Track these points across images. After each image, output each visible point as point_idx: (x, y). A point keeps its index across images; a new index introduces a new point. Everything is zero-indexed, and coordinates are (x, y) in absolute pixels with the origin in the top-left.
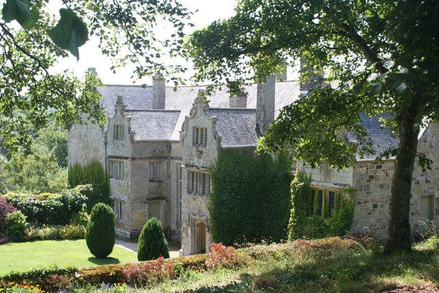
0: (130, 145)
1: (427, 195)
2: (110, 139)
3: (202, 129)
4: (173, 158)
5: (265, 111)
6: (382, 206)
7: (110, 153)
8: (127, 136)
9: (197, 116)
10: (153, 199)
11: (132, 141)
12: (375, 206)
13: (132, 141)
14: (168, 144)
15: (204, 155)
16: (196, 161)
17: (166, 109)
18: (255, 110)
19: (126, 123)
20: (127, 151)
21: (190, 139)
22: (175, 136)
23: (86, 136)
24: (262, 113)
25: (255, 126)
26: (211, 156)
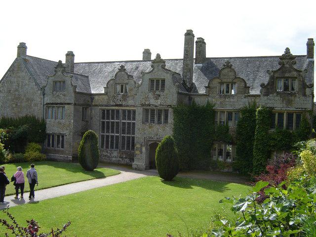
0: (73, 95)
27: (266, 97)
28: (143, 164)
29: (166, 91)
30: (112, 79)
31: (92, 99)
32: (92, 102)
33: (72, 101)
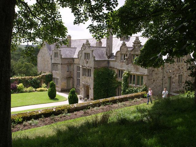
0: (60, 59)
1: (170, 76)
2: (53, 57)
3: (88, 54)
4: (75, 64)
5: (109, 48)
6: (156, 81)
7: (53, 62)
8: (60, 56)
9: (86, 49)
10: (68, 78)
11: (61, 58)
12: (154, 81)
13: (61, 58)
14: (73, 59)
15: (89, 63)
16: (85, 65)
17: (71, 47)
18: (105, 47)
19: (59, 52)
20: (59, 61)
21: (83, 57)
22: (75, 56)
23: (44, 56)
24: (108, 48)
25: (106, 53)
26: (91, 64)
27: (127, 66)
28: (122, 117)
29: (90, 60)
30: (80, 51)
31: (74, 60)
32: (74, 62)
33: (60, 63)
